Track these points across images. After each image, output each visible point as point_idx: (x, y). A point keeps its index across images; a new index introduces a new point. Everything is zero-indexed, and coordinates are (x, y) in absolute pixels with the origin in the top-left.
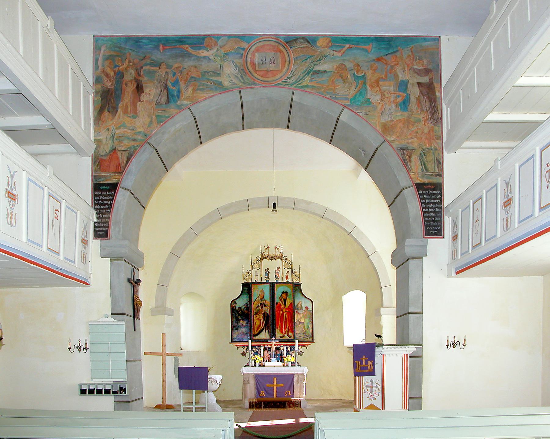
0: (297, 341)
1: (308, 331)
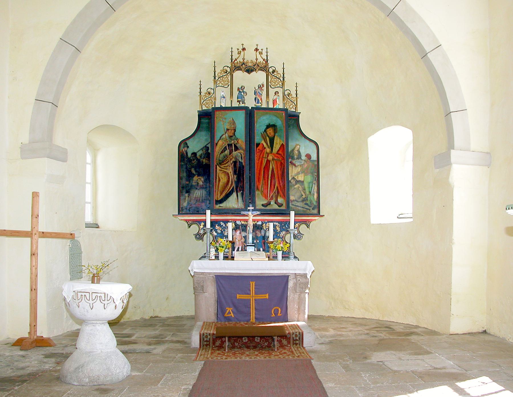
0: (292, 213)
1: (310, 197)
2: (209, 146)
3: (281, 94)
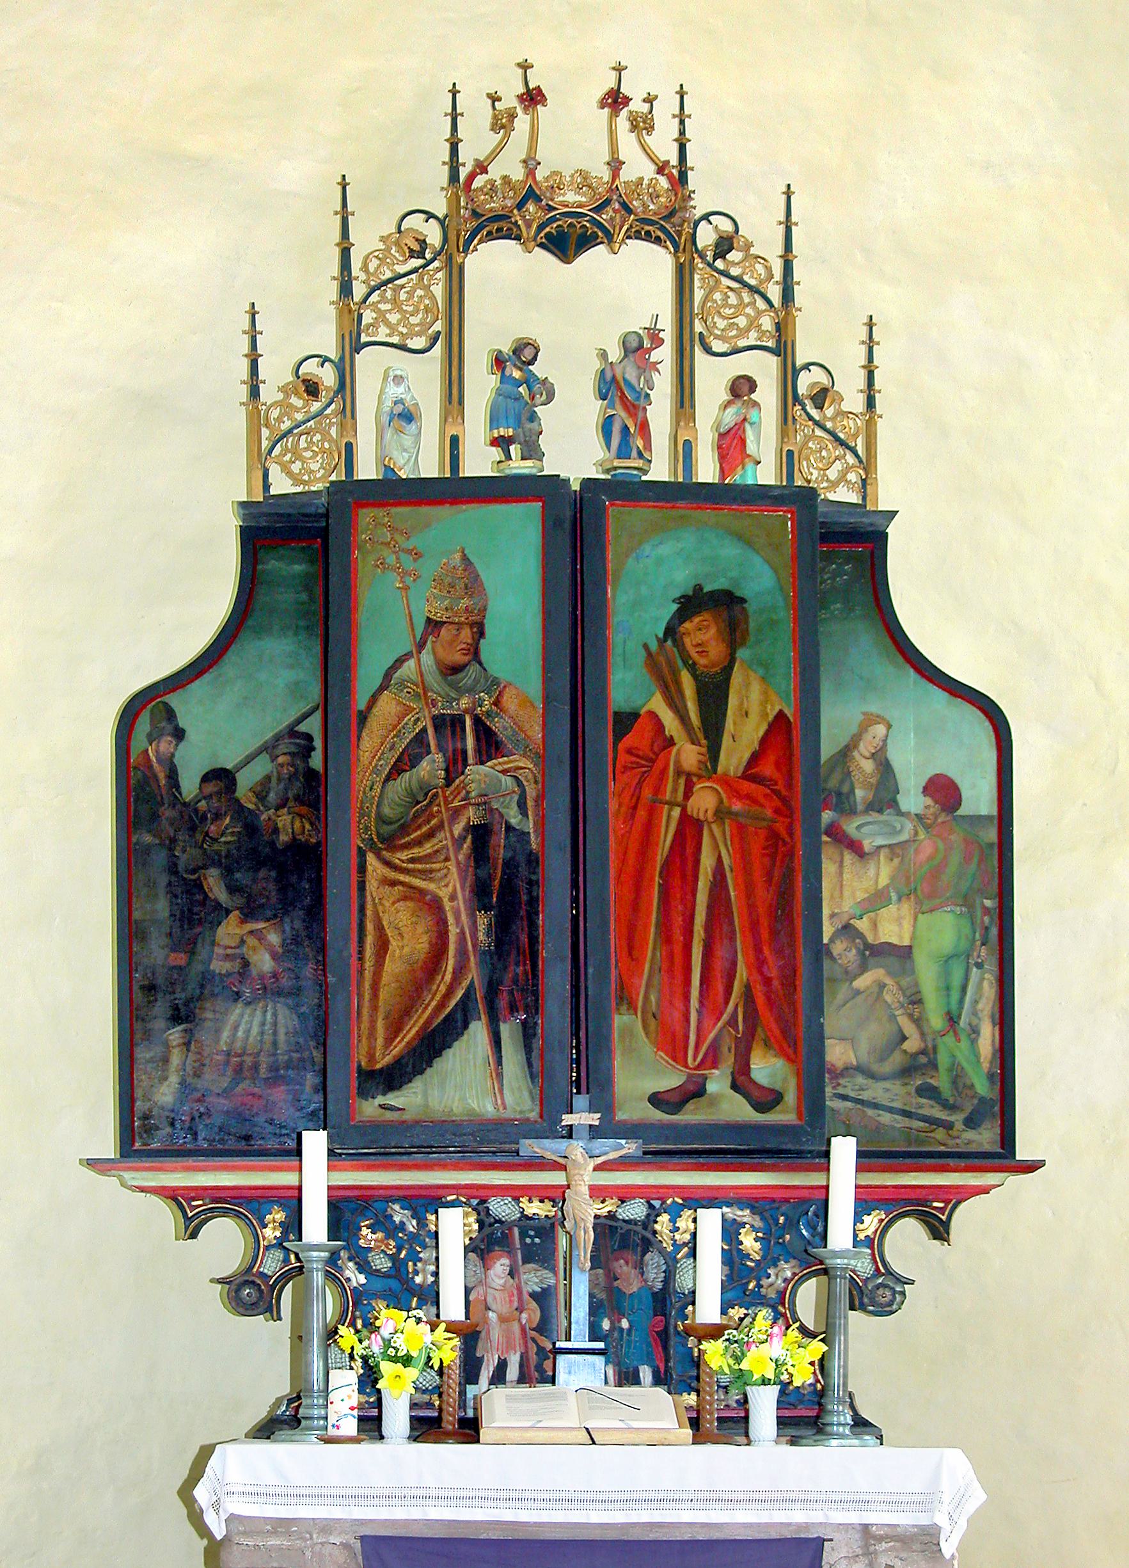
0: (844, 1150)
1: (950, 1050)
2: (312, 726)
3: (767, 395)
